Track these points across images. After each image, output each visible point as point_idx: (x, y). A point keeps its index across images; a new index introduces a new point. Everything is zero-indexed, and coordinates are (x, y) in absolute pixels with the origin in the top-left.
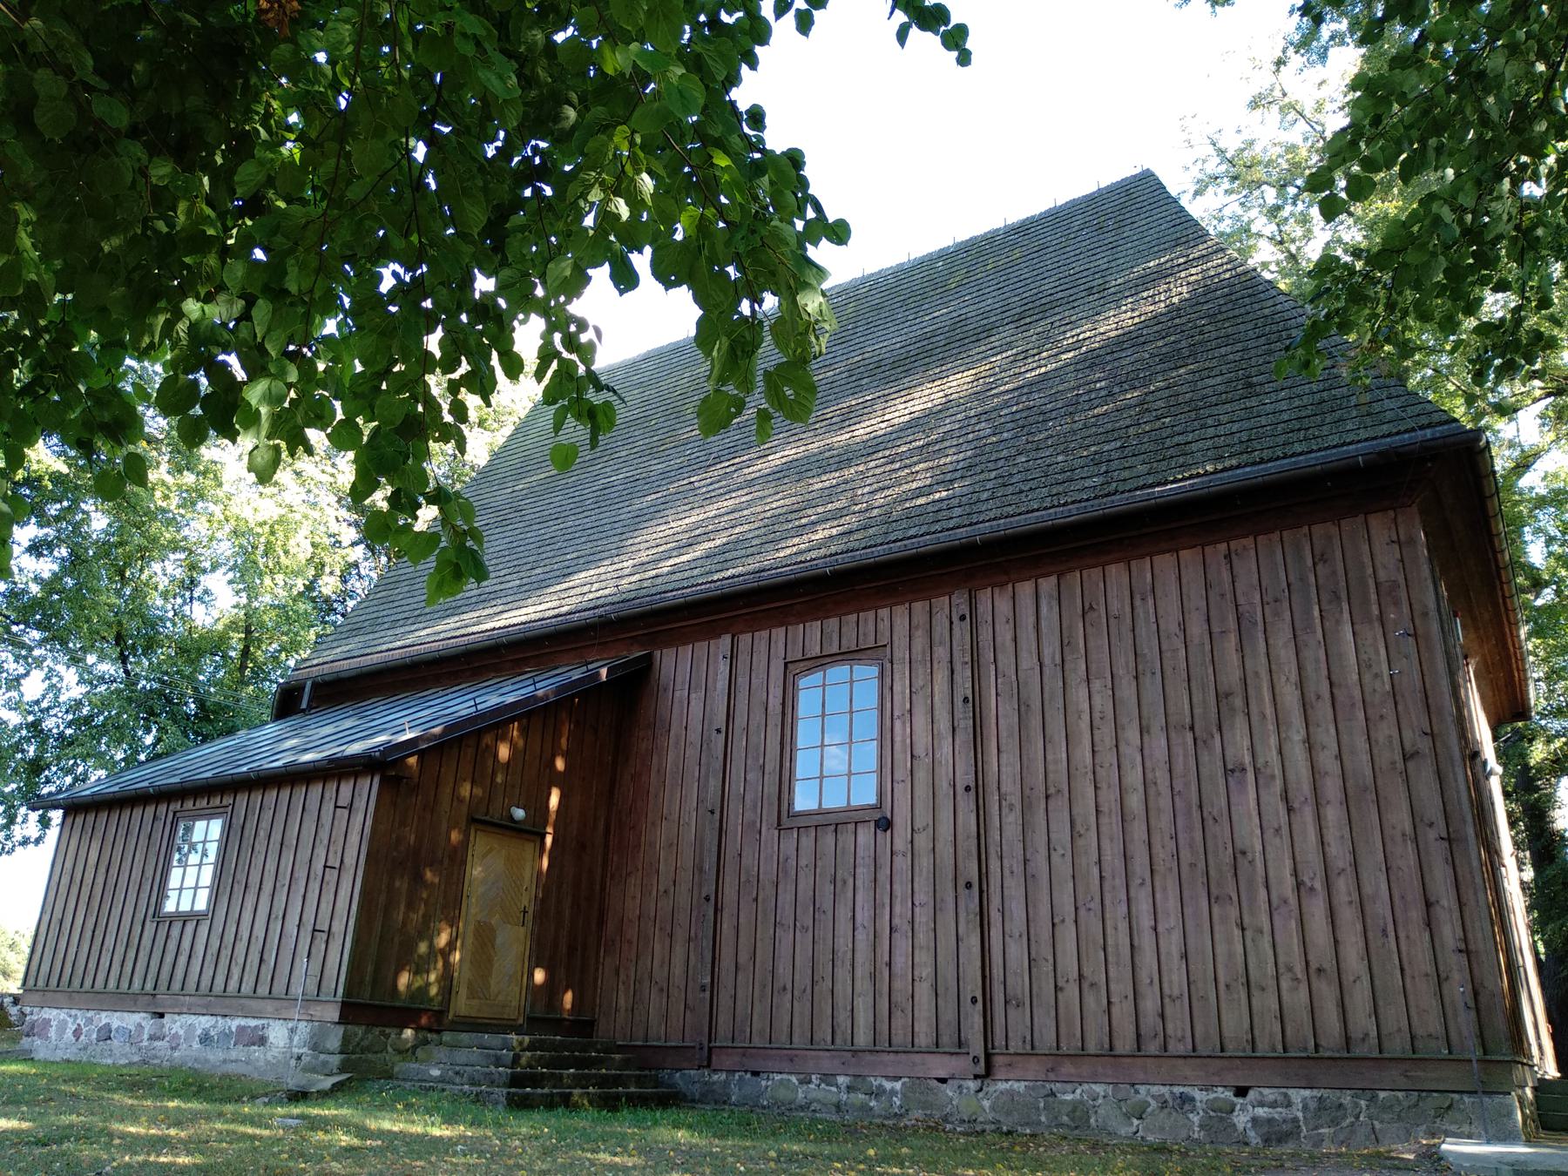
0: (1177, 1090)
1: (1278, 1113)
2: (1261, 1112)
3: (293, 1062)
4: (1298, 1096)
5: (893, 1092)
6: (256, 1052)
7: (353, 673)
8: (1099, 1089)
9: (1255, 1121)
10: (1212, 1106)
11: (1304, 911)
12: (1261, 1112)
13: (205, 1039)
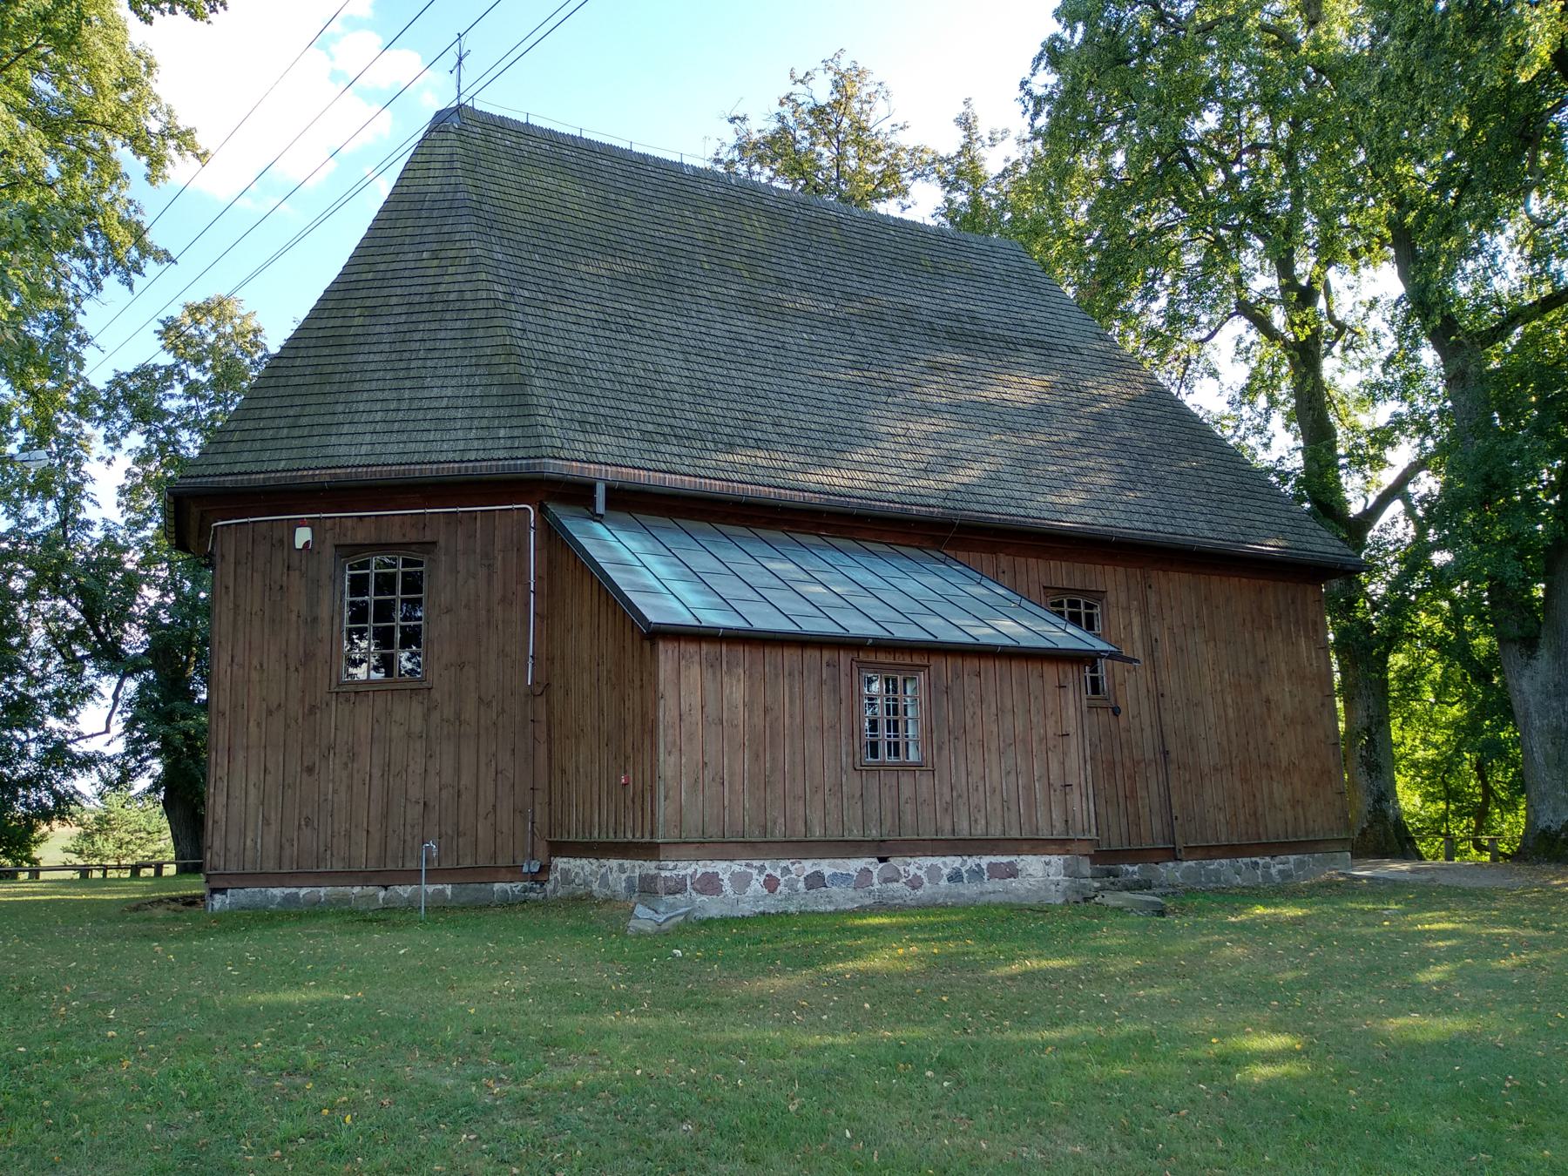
0: (1254, 859)
4: (1292, 858)
6: (1013, 883)
7: (634, 487)
8: (1224, 861)
9: (1280, 872)
11: (791, 656)
12: (1281, 867)
13: (955, 877)
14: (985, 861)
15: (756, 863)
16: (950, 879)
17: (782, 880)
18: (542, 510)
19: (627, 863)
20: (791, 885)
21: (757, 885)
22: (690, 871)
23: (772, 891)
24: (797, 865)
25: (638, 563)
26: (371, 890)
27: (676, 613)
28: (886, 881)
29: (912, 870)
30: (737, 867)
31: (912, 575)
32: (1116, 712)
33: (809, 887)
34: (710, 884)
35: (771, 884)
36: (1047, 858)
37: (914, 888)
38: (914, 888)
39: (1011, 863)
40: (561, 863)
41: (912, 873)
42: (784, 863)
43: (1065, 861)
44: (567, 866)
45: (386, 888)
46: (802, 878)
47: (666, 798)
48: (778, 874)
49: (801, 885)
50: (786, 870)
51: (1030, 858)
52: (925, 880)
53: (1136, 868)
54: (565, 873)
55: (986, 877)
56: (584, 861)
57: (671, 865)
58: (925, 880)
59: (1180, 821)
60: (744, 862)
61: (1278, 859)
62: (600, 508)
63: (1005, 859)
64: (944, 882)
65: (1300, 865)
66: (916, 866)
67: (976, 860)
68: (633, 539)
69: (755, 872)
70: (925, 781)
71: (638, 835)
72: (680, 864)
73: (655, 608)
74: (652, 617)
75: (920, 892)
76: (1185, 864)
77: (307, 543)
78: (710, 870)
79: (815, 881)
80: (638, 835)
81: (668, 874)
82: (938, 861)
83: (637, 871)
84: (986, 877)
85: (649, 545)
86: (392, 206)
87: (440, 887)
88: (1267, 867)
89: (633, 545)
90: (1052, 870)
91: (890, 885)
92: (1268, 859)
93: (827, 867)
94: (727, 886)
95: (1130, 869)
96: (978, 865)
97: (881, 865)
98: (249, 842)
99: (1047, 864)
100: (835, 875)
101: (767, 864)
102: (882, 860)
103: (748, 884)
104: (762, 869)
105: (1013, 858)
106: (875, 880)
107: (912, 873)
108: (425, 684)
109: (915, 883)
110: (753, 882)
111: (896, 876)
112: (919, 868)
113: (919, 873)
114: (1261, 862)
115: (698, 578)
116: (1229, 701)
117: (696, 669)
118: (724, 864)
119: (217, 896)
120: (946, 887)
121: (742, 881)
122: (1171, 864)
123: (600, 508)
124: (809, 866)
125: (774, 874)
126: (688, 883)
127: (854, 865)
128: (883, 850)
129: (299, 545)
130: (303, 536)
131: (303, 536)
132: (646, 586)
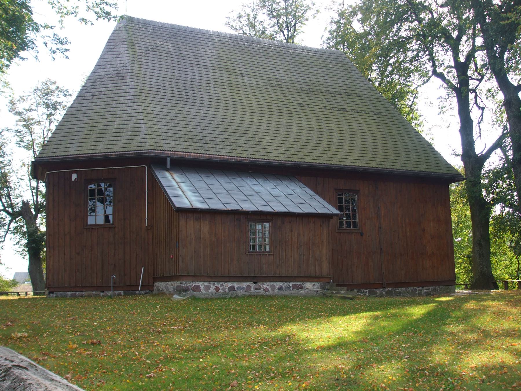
0: (415, 288)
1: (428, 291)
2: (426, 291)
3: (316, 293)
4: (431, 288)
5: (366, 292)
6: (302, 291)
8: (403, 289)
10: (419, 290)
12: (426, 291)
13: (281, 288)
14: (291, 284)
15: (212, 283)
16: (279, 289)
17: (221, 288)
18: (149, 167)
19: (173, 283)
20: (224, 289)
21: (212, 289)
22: (191, 284)
23: (217, 291)
24: (226, 284)
25: (178, 186)
26: (98, 293)
27: (185, 204)
28: (256, 289)
29: (265, 286)
30: (206, 284)
31: (278, 187)
32: (362, 234)
33: (230, 291)
34: (197, 289)
35: (217, 289)
36: (314, 283)
37: (266, 292)
38: (266, 292)
39: (300, 285)
40: (157, 284)
41: (265, 287)
42: (221, 283)
43: (320, 284)
44: (158, 285)
45: (103, 292)
46: (227, 288)
47: (182, 262)
48: (219, 286)
49: (227, 290)
50: (222, 285)
51: (309, 283)
52: (270, 289)
53: (367, 291)
54: (158, 287)
55: (291, 289)
56: (163, 283)
57: (184, 283)
58: (270, 289)
59: (385, 274)
60: (208, 282)
61: (425, 288)
62: (168, 167)
63: (298, 283)
64: (276, 290)
65: (434, 290)
66: (266, 285)
67: (288, 284)
68: (178, 177)
69: (212, 286)
70: (271, 258)
71: (173, 273)
72: (187, 282)
73: (179, 202)
74: (178, 205)
75: (268, 293)
76: (387, 289)
77: (76, 179)
78: (197, 284)
79: (232, 289)
80: (173, 273)
81: (183, 285)
82: (275, 284)
83: (176, 284)
84: (291, 289)
85: (184, 179)
86: (113, 34)
87: (120, 292)
88: (420, 291)
89: (178, 179)
90: (315, 287)
91: (257, 291)
92: (421, 288)
93: (236, 285)
94: (202, 288)
95: (365, 291)
96: (289, 285)
97: (254, 284)
98: (60, 277)
99: (314, 285)
100: (238, 287)
101: (216, 283)
102: (255, 283)
103: (209, 289)
104: (214, 285)
105: (301, 283)
106: (252, 289)
107: (265, 287)
108: (114, 226)
109: (266, 290)
110: (211, 288)
111: (259, 288)
112: (268, 286)
113: (268, 287)
114: (418, 289)
115: (196, 190)
116: (408, 230)
117: (192, 221)
118: (201, 283)
119: (51, 294)
120: (277, 292)
121: (207, 288)
122: (382, 289)
123: (168, 167)
124: (230, 285)
125: (218, 286)
126: (190, 288)
127: (245, 285)
128: (255, 280)
129: (73, 179)
130: (74, 177)
131: (74, 177)
132: (178, 194)
